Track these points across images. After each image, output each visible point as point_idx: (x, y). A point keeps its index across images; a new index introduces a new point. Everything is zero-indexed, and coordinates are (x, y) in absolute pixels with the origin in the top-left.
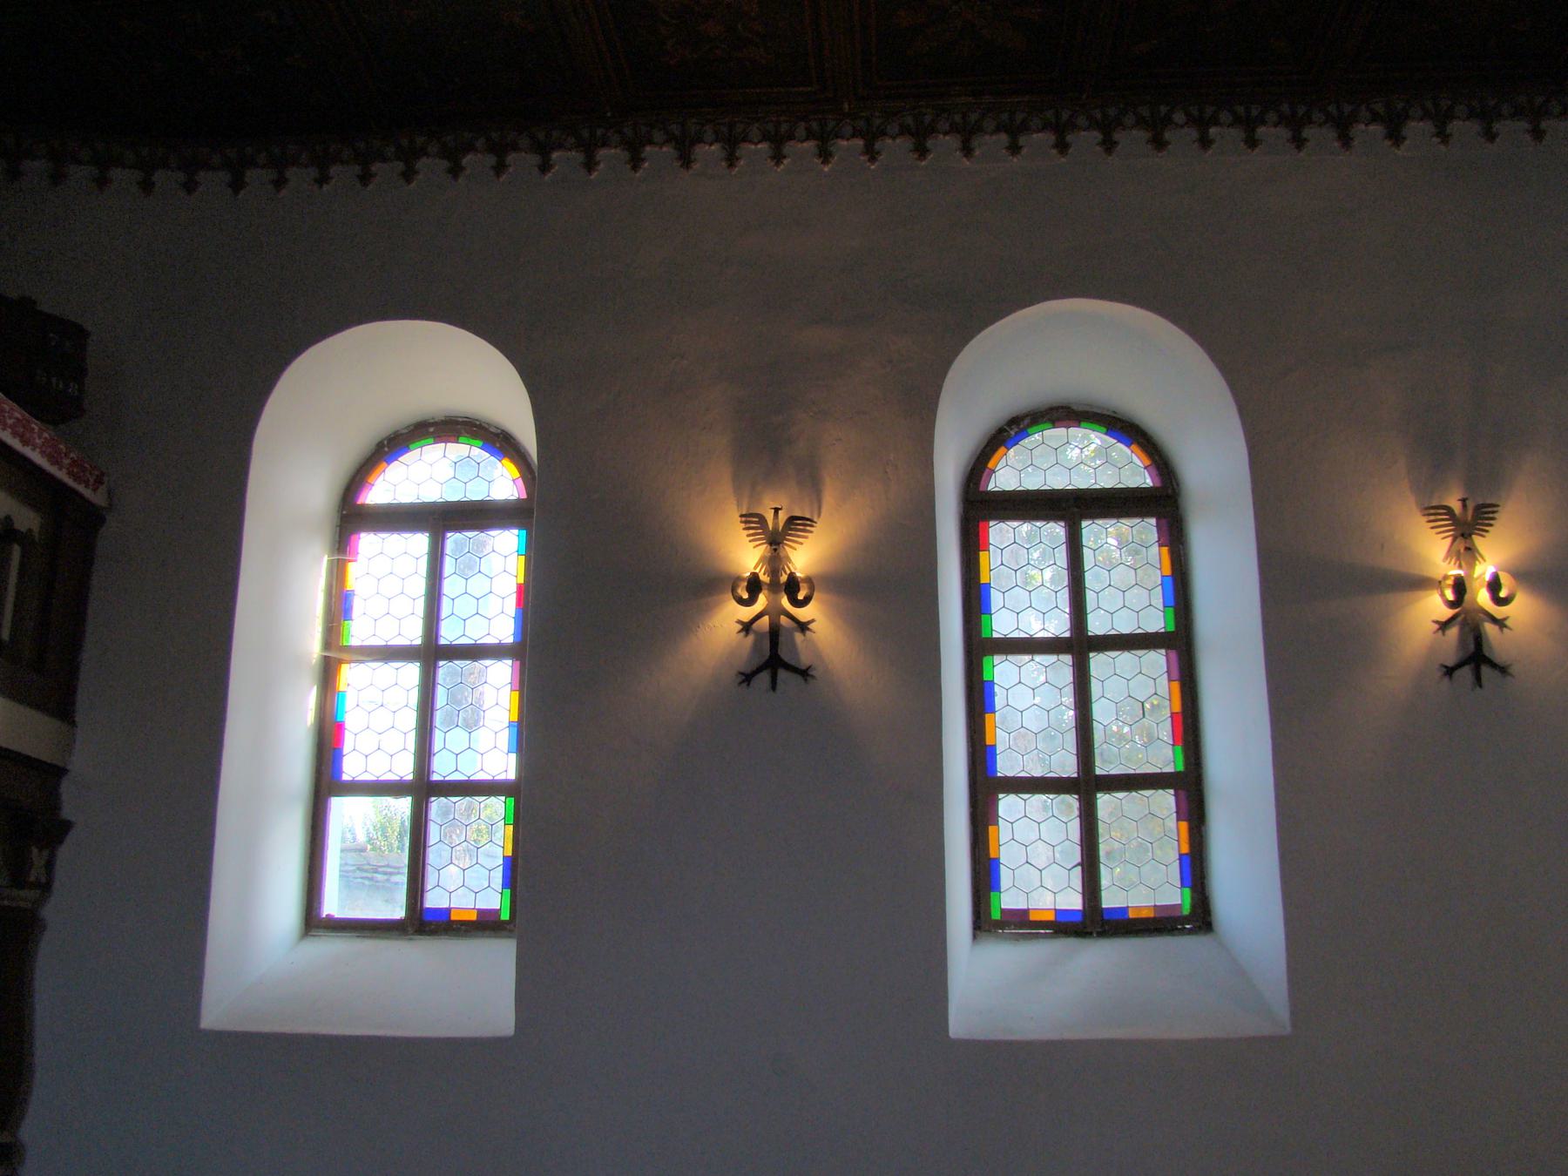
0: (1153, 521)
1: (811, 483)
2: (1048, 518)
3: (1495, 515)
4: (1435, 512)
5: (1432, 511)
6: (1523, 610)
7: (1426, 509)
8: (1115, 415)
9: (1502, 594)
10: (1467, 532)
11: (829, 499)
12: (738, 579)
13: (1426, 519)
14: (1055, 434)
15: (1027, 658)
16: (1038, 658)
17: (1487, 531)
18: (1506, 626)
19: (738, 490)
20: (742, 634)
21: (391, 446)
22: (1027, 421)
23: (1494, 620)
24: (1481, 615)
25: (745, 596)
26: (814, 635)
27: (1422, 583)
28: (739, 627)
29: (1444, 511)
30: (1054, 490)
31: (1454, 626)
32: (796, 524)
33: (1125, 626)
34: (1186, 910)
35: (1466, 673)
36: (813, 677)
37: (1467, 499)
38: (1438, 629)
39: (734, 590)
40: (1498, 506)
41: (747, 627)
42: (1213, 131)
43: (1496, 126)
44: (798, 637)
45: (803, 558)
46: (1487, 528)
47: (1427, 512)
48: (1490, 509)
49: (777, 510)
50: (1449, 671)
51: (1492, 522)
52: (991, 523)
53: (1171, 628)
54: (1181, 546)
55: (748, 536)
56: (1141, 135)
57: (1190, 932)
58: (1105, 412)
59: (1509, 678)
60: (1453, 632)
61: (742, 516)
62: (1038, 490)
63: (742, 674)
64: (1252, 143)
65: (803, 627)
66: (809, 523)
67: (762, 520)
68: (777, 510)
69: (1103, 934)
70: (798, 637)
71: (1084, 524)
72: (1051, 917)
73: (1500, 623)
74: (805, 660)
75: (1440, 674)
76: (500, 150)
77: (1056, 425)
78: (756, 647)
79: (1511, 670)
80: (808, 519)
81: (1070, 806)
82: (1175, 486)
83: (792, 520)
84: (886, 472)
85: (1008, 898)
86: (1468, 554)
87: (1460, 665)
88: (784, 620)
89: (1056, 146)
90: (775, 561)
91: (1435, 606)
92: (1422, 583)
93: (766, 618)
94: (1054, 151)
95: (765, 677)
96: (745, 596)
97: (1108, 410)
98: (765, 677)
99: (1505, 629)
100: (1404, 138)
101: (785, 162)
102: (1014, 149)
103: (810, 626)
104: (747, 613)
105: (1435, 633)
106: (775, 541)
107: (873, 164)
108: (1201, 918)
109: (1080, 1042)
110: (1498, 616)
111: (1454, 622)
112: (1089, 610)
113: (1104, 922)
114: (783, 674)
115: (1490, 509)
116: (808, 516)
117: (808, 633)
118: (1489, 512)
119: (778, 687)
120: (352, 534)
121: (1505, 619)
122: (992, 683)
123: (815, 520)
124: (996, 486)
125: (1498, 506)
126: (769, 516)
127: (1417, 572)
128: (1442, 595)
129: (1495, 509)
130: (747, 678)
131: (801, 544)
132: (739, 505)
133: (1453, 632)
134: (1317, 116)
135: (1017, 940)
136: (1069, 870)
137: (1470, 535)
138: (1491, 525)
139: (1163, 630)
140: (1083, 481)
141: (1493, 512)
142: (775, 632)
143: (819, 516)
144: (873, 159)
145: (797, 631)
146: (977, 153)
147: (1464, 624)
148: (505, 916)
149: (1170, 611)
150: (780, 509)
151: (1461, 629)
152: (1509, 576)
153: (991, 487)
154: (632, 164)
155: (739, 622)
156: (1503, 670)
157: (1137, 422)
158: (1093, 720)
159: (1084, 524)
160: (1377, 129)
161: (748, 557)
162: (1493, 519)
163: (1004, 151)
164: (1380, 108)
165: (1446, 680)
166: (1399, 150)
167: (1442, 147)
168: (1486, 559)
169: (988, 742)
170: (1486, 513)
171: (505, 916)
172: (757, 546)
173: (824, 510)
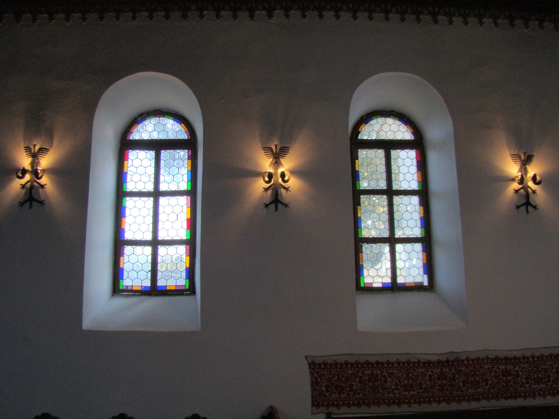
0: (415, 151)
1: (50, 136)
2: (379, 148)
3: (289, 151)
4: (268, 149)
5: (267, 149)
6: (293, 183)
7: (263, 148)
8: (176, 113)
9: (286, 179)
10: (277, 157)
11: (55, 142)
12: (19, 170)
13: (264, 151)
14: (381, 120)
15: (147, 198)
16: (142, 198)
17: (285, 156)
18: (289, 190)
19: (25, 140)
20: (22, 189)
21: (366, 119)
22: (145, 115)
23: (284, 188)
24: (280, 186)
25: (21, 175)
26: (46, 189)
27: (259, 174)
28: (21, 186)
29: (269, 149)
30: (170, 139)
31: (270, 190)
32: (43, 150)
33: (173, 188)
34: (187, 287)
35: (273, 206)
36: (44, 204)
37: (526, 153)
38: (264, 191)
39: (17, 173)
40: (289, 148)
41: (23, 186)
42: (205, 12)
43: (373, 15)
44: (41, 190)
45: (45, 162)
46: (285, 155)
47: (264, 149)
48: (287, 149)
49: (276, 146)
50: (267, 206)
51: (287, 153)
52: (130, 151)
53: (189, 189)
54: (196, 160)
55: (26, 154)
56: (179, 13)
57: (188, 295)
58: (174, 112)
59: (288, 208)
60: (270, 192)
61: (24, 147)
62: (165, 139)
63: (265, 204)
64: (218, 16)
65: (42, 186)
66: (48, 150)
67: (271, 149)
68: (35, 145)
69: (156, 295)
70: (41, 190)
71: (162, 151)
72: (140, 289)
73: (287, 189)
74: (42, 198)
75: (263, 206)
76: (450, 16)
77: (156, 116)
78: (26, 194)
79: (289, 206)
80: (48, 149)
81: (366, 248)
82: (195, 138)
83: (41, 149)
84: (76, 132)
85: (126, 282)
86: (277, 163)
87: (271, 203)
88: (35, 184)
89: (149, 17)
90: (34, 164)
91: (261, 184)
92: (259, 174)
93: (29, 183)
94: (148, 19)
95: (28, 204)
96: (21, 175)
97: (175, 111)
98: (28, 204)
99: (288, 191)
100: (273, 16)
101: (54, 21)
102: (134, 18)
103: (289, 189)
104: (23, 181)
105: (263, 192)
106: (35, 156)
107: (84, 23)
108: (431, 287)
109: (129, 332)
110: (286, 187)
111: (270, 188)
112: (393, 180)
113: (157, 291)
114: (34, 203)
115: (287, 149)
116: (48, 148)
117: (44, 188)
118: (287, 150)
119: (32, 208)
120: (125, 150)
121: (289, 188)
122: (125, 207)
123: (50, 149)
124: (403, 138)
125: (289, 148)
126: (32, 147)
127: (259, 170)
128: (264, 178)
129: (289, 149)
130: (22, 204)
131: (44, 157)
132: (25, 143)
133: (270, 192)
134: (345, 8)
135: (127, 297)
136: (147, 272)
137: (278, 158)
138: (287, 154)
139: (186, 189)
140: (390, 136)
141: (288, 150)
142: (32, 187)
143: (52, 147)
144: (84, 21)
145: (40, 188)
146: (121, 19)
147: (273, 189)
148: (426, 283)
149: (190, 183)
150: (36, 145)
151: (272, 191)
152: (289, 172)
153: (131, 138)
154: (86, 20)
155: (21, 185)
156: (286, 205)
157: (184, 116)
158: (394, 219)
159: (162, 151)
160: (264, 13)
161: (26, 162)
162: (288, 152)
163: (131, 19)
164: (351, 6)
165: (266, 208)
166: (118, 21)
167: (286, 20)
168: (284, 166)
169: (122, 228)
170: (282, 154)
171: (426, 283)
172: (269, 159)
173: (53, 146)
